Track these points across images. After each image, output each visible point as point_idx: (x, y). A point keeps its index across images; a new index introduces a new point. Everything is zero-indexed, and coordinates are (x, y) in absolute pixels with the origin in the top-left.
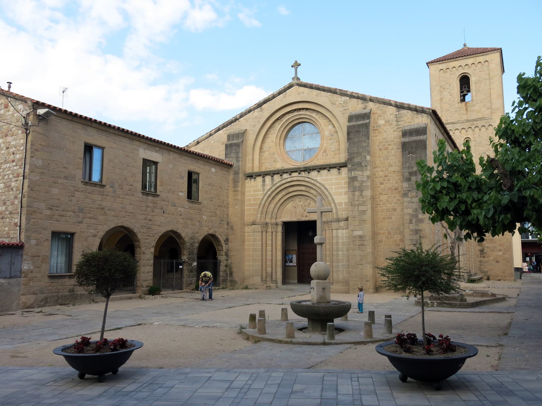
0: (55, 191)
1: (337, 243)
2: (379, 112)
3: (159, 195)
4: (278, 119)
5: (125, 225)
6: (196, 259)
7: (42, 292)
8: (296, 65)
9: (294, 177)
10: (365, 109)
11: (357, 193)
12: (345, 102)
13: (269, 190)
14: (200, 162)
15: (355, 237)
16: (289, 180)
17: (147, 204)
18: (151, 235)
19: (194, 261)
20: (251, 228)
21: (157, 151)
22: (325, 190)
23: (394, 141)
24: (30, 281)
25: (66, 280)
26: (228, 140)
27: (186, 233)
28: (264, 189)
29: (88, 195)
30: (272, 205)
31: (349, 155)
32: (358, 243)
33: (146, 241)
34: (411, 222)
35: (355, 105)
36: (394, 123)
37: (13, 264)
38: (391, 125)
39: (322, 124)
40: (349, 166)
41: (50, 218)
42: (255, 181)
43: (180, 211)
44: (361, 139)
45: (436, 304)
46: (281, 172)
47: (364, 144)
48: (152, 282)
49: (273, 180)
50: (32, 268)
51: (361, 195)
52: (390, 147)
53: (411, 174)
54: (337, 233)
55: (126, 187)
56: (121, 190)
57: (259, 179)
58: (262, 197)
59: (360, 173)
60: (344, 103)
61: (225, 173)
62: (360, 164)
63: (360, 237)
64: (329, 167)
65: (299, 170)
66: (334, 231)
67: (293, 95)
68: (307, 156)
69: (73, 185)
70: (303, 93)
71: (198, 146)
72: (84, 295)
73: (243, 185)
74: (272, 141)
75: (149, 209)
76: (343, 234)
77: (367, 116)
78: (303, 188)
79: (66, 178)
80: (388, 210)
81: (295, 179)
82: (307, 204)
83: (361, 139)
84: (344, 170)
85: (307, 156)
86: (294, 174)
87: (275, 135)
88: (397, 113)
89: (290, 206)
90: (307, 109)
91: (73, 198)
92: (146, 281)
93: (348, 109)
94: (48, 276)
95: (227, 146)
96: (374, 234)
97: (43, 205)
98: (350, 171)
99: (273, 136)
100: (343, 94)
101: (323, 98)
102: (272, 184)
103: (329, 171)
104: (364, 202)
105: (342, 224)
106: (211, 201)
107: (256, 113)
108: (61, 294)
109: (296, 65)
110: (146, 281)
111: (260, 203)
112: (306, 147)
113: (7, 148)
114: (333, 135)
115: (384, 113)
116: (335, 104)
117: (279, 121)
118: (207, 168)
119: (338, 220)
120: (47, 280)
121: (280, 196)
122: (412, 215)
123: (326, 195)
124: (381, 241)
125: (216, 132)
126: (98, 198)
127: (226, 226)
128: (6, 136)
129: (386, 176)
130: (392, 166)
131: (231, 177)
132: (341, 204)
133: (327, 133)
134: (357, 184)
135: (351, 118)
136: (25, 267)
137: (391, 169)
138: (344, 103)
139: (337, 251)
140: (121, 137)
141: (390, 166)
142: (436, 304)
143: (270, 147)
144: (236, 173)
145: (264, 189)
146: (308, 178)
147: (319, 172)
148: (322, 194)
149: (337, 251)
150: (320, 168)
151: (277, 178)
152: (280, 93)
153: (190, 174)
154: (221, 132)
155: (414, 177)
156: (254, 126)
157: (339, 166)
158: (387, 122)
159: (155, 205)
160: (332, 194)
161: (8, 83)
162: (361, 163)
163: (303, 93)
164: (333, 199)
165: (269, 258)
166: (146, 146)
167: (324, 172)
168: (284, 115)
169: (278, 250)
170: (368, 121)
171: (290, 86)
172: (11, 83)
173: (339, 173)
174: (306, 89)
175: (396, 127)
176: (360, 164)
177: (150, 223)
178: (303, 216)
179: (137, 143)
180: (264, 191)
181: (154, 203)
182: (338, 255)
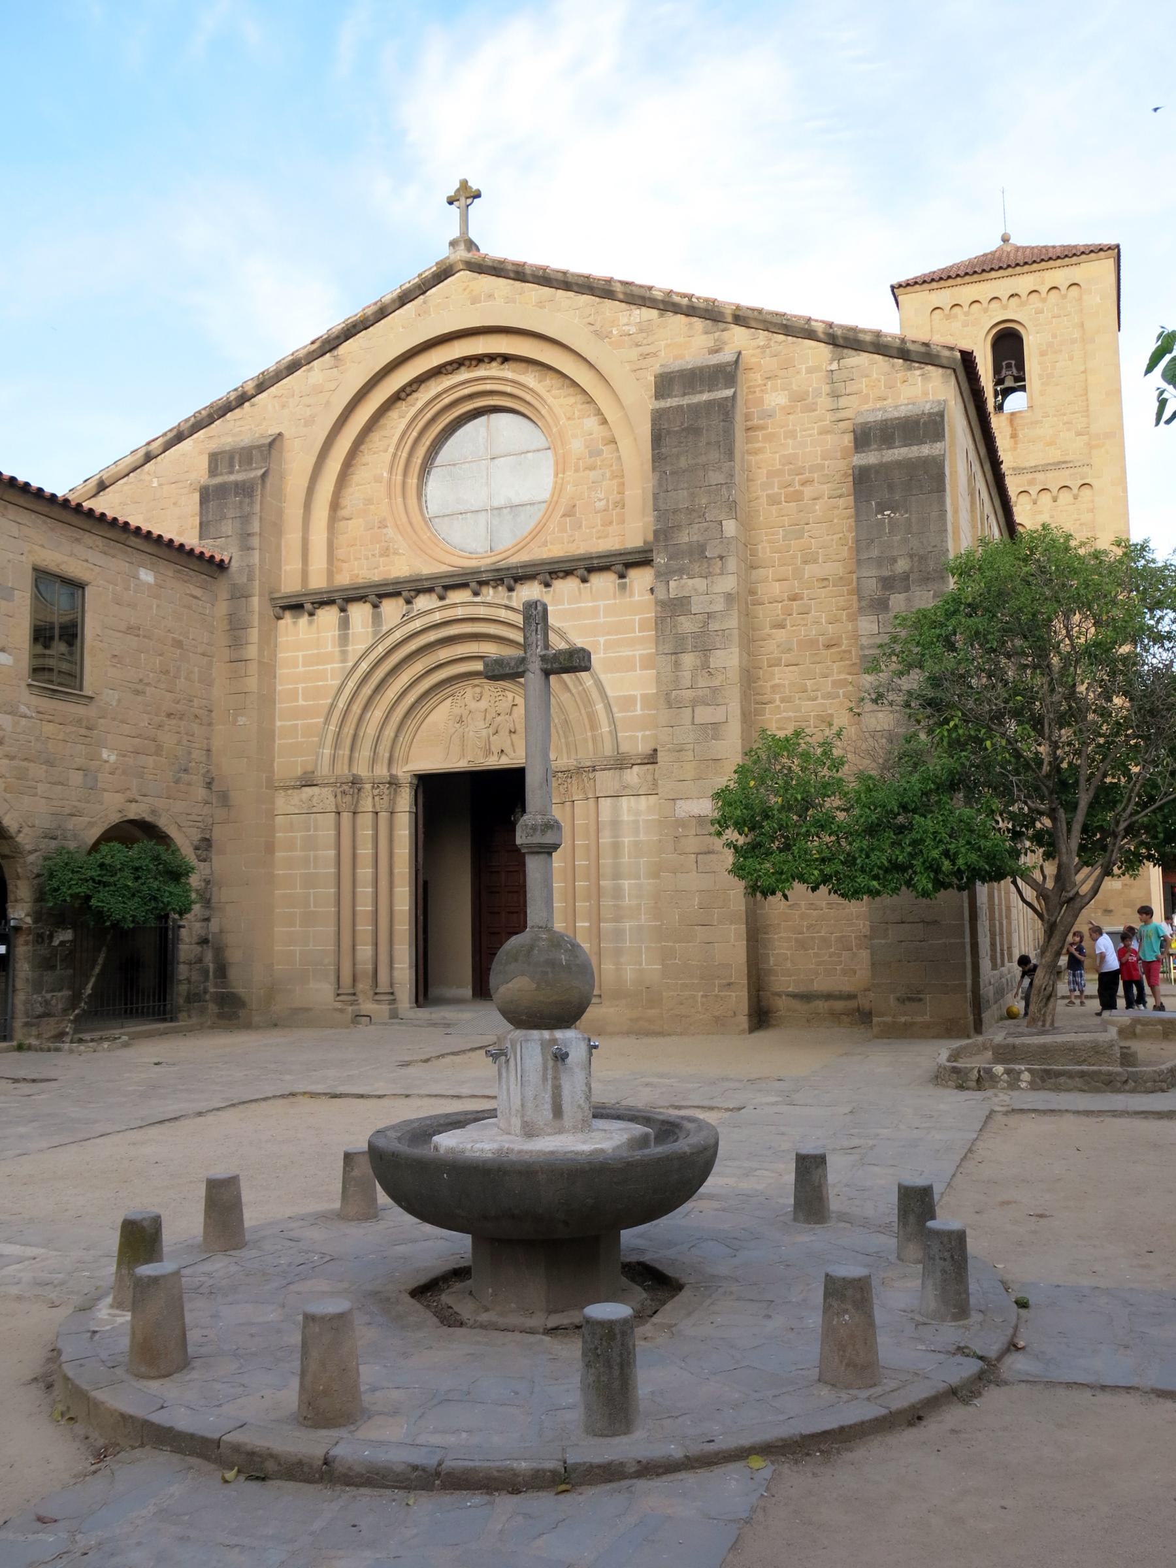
1: (616, 847)
2: (769, 363)
4: (398, 397)
9: (454, 605)
10: (715, 351)
13: (362, 657)
14: (89, 539)
15: (681, 823)
23: (822, 467)
26: (213, 471)
28: (344, 653)
30: (377, 714)
31: (658, 519)
36: (824, 402)
40: (660, 559)
42: (310, 623)
44: (702, 460)
45: (1026, 1076)
49: (377, 619)
51: (705, 666)
52: (808, 491)
53: (888, 584)
54: (616, 810)
57: (328, 616)
59: (699, 584)
60: (641, 331)
61: (198, 592)
62: (698, 552)
66: (605, 804)
67: (459, 304)
70: (490, 296)
73: (269, 640)
81: (460, 612)
83: (702, 460)
87: (388, 457)
88: (834, 366)
89: (441, 714)
90: (505, 358)
93: (655, 354)
95: (206, 495)
98: (664, 576)
102: (375, 633)
103: (584, 580)
104: (714, 690)
106: (137, 692)
109: (466, 195)
117: (402, 406)
119: (621, 763)
121: (405, 678)
127: (201, 793)
129: (794, 598)
130: (815, 561)
131: (222, 608)
132: (628, 702)
134: (687, 625)
135: (665, 384)
137: (809, 570)
138: (641, 331)
143: (369, 501)
144: (239, 595)
145: (344, 653)
146: (507, 607)
147: (547, 585)
149: (617, 876)
151: (392, 609)
155: (902, 596)
157: (623, 563)
158: (799, 398)
162: (702, 548)
163: (490, 296)
171: (443, 273)
173: (623, 587)
175: (829, 416)
176: (698, 552)
178: (488, 752)
180: (344, 661)
182: (617, 893)
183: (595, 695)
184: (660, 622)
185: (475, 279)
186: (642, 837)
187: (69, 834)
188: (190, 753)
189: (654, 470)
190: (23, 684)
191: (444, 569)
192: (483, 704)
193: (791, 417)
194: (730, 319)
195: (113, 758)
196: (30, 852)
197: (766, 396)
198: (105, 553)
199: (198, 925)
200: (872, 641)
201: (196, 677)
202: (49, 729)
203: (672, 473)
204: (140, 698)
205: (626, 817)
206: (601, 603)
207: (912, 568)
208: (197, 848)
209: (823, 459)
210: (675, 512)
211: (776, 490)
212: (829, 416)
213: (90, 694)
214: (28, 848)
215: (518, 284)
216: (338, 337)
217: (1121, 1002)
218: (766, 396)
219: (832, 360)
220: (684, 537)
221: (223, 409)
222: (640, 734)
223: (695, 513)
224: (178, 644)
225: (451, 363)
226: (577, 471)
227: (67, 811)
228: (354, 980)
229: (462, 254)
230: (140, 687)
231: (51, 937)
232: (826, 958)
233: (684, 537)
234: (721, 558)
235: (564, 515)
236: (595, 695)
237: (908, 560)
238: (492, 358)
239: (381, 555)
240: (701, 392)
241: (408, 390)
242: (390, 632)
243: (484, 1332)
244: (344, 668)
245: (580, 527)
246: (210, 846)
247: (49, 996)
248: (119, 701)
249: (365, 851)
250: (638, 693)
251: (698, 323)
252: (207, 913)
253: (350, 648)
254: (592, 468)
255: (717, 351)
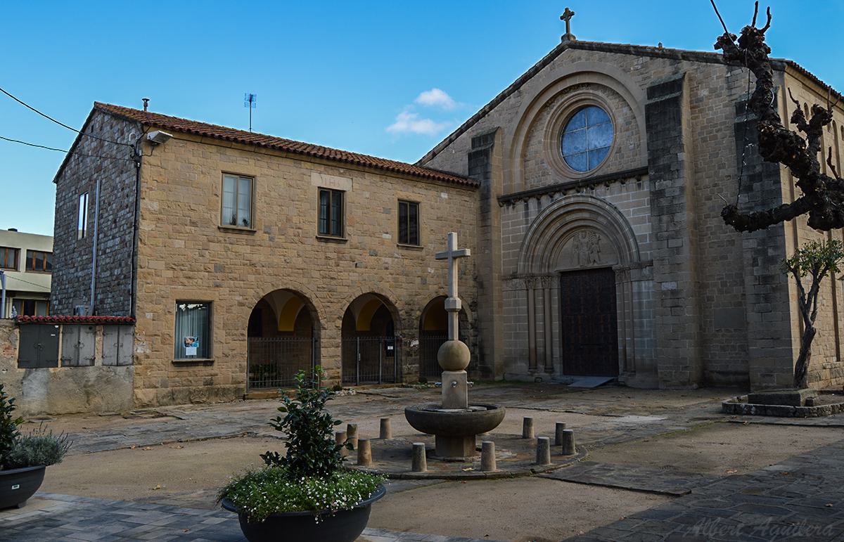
0: (179, 244)
1: (640, 304)
2: (699, 76)
3: (347, 241)
4: (546, 106)
5: (291, 287)
6: (417, 335)
7: (164, 385)
8: (567, 15)
10: (675, 73)
11: (665, 218)
12: (644, 66)
13: (534, 222)
14: (420, 185)
15: (664, 293)
16: (563, 203)
17: (328, 255)
18: (335, 301)
19: (413, 338)
20: (510, 285)
21: (341, 175)
22: (618, 216)
23: (725, 123)
24: (147, 369)
25: (201, 368)
26: (473, 147)
27: (398, 295)
28: (527, 221)
29: (230, 246)
31: (650, 154)
32: (669, 303)
33: (328, 309)
34: (755, 263)
35: (660, 69)
36: (725, 92)
37: (122, 346)
38: (718, 96)
39: (612, 106)
40: (652, 173)
41: (172, 281)
43: (386, 263)
44: (667, 126)
45: (753, 409)
46: (550, 191)
47: (674, 134)
48: (340, 370)
49: (539, 203)
50: (148, 351)
51: (672, 220)
52: (719, 134)
53: (753, 178)
54: (639, 287)
55: (291, 232)
56: (282, 237)
57: (520, 205)
58: (524, 233)
59: (668, 183)
60: (642, 67)
61: (467, 199)
62: (667, 168)
63: (673, 292)
64: (621, 177)
65: (577, 186)
66: (635, 284)
67: (564, 66)
68: (595, 162)
69: (205, 233)
70: (580, 58)
71: (435, 159)
72: (228, 389)
74: (540, 142)
75: (330, 262)
76: (649, 288)
77: (676, 85)
78: (586, 215)
79: (193, 224)
80: (62, 271)
81: (572, 200)
82: (595, 240)
83: (667, 126)
84: (645, 181)
85: (595, 162)
86: (571, 193)
87: (543, 132)
88: (729, 75)
89: (569, 244)
90: (588, 84)
91: (207, 252)
92: (328, 369)
93: (649, 77)
94: (173, 363)
95: (470, 156)
96: (700, 286)
97: (161, 265)
98: (653, 180)
99: (540, 135)
100: (639, 51)
101: (609, 64)
102: (539, 211)
103: (623, 183)
104: (677, 232)
105: (646, 271)
107: (512, 100)
108: (194, 388)
109: (567, 15)
110: (328, 369)
111: (523, 244)
112: (592, 147)
113: (123, 189)
114: (630, 123)
115: (708, 76)
116: (630, 70)
118: (432, 193)
119: (640, 266)
120: (172, 368)
121: (552, 230)
122: (757, 251)
123: (619, 225)
124: (710, 299)
125: (457, 136)
126: (245, 250)
128: (122, 172)
129: (715, 185)
130: (724, 168)
132: (644, 237)
133: (620, 121)
134: (664, 202)
135: (652, 91)
136: (639, 358)
137: (723, 172)
138: (642, 67)
139: (641, 317)
140: (280, 159)
141: (722, 166)
142: (753, 409)
143: (536, 152)
145: (527, 221)
146: (591, 197)
147: (608, 186)
148: (614, 226)
149: (641, 317)
150: (607, 180)
152: (545, 63)
153: (403, 204)
154: (464, 135)
155: (758, 184)
156: (511, 121)
157: (638, 174)
158: (712, 91)
159: (341, 255)
160: (631, 223)
161: (143, 100)
162: (669, 166)
163: (580, 58)
164: (631, 229)
165: (540, 331)
166: (322, 168)
167: (615, 186)
168: (555, 98)
169: (554, 319)
170: (678, 94)
171: (560, 50)
172: (147, 100)
174: (583, 51)
175: (728, 99)
176: (667, 168)
177: (333, 282)
178: (589, 261)
179: (308, 165)
180: (527, 223)
181: (339, 252)
182: (641, 325)
183: (629, 235)
184: (652, 202)
185: (572, 52)
186: (651, 299)
187: (415, 303)
188: (466, 266)
189: (647, 132)
190: (395, 246)
191: (568, 180)
192: (586, 240)
193: (710, 101)
194: (681, 58)
195: (433, 272)
196: (401, 310)
197: (699, 92)
198: (426, 189)
199: (472, 338)
200: (745, 206)
201: (467, 234)
202: (406, 262)
203: (655, 133)
204: (443, 246)
205: (644, 290)
206: (630, 193)
207: (763, 170)
208: (470, 306)
209: (726, 118)
210: (657, 151)
211: (705, 135)
212: (728, 99)
213: (423, 246)
214: (400, 309)
215: (591, 52)
216: (520, 83)
217: (59, 366)
218: (699, 92)
219: (727, 72)
220: (662, 162)
221: (477, 118)
222: (649, 252)
223: (666, 150)
224: (459, 222)
225: (566, 89)
226: (621, 132)
227: (414, 294)
228: (536, 362)
229: (566, 42)
230: (443, 241)
231: (410, 343)
232: (734, 355)
233: (662, 162)
234: (678, 170)
235: (617, 153)
236: (629, 235)
237: (761, 166)
238: (583, 85)
239: (542, 176)
240: (667, 94)
241: (550, 102)
242: (544, 210)
243: (493, 481)
244: (527, 227)
245: (623, 158)
246: (477, 305)
247: (409, 366)
248: (434, 248)
249: (540, 306)
250: (647, 233)
251: (667, 61)
252: (476, 333)
253: (529, 218)
254: (627, 130)
255: (676, 73)
